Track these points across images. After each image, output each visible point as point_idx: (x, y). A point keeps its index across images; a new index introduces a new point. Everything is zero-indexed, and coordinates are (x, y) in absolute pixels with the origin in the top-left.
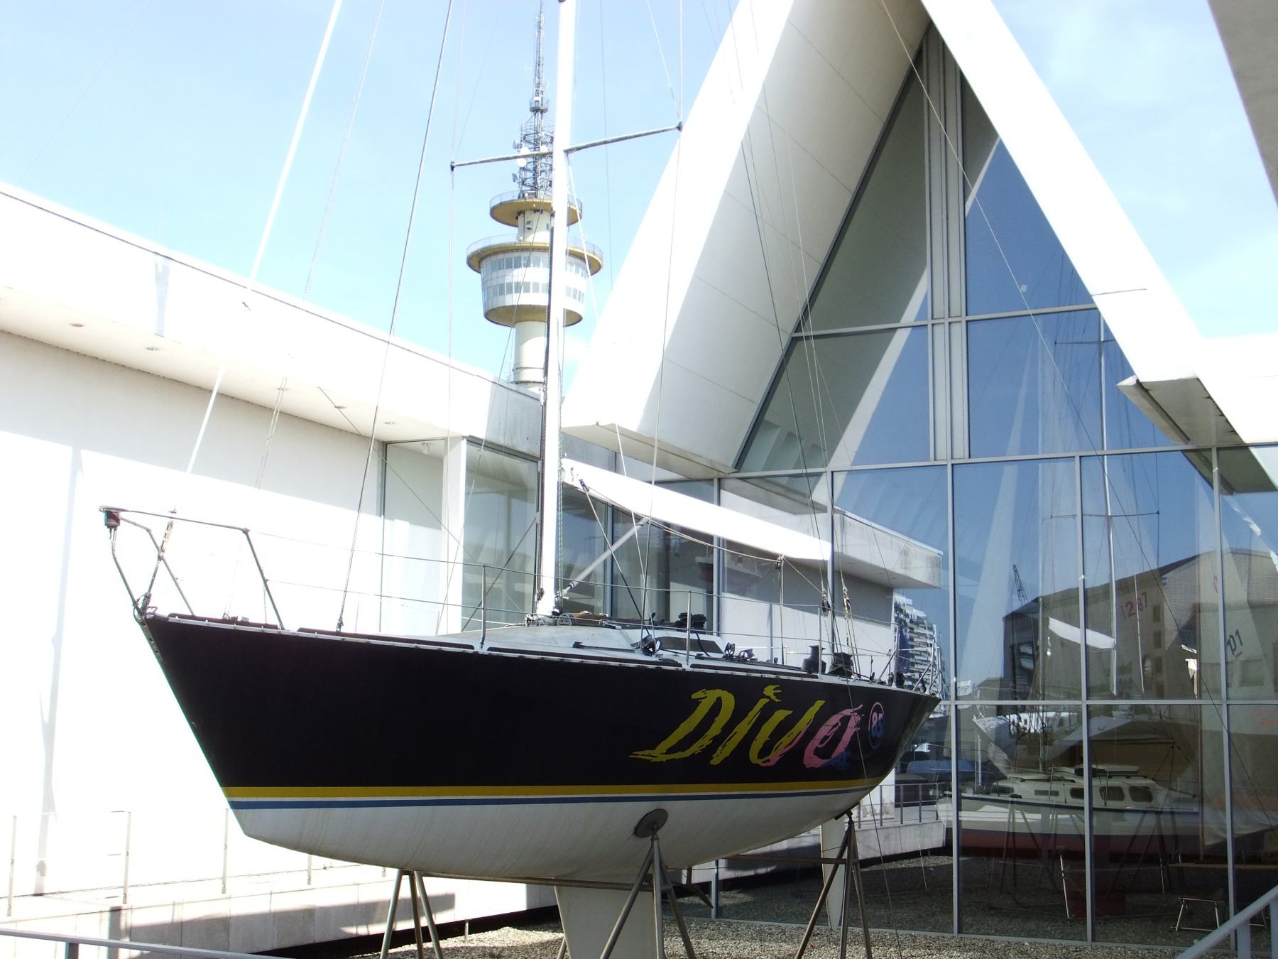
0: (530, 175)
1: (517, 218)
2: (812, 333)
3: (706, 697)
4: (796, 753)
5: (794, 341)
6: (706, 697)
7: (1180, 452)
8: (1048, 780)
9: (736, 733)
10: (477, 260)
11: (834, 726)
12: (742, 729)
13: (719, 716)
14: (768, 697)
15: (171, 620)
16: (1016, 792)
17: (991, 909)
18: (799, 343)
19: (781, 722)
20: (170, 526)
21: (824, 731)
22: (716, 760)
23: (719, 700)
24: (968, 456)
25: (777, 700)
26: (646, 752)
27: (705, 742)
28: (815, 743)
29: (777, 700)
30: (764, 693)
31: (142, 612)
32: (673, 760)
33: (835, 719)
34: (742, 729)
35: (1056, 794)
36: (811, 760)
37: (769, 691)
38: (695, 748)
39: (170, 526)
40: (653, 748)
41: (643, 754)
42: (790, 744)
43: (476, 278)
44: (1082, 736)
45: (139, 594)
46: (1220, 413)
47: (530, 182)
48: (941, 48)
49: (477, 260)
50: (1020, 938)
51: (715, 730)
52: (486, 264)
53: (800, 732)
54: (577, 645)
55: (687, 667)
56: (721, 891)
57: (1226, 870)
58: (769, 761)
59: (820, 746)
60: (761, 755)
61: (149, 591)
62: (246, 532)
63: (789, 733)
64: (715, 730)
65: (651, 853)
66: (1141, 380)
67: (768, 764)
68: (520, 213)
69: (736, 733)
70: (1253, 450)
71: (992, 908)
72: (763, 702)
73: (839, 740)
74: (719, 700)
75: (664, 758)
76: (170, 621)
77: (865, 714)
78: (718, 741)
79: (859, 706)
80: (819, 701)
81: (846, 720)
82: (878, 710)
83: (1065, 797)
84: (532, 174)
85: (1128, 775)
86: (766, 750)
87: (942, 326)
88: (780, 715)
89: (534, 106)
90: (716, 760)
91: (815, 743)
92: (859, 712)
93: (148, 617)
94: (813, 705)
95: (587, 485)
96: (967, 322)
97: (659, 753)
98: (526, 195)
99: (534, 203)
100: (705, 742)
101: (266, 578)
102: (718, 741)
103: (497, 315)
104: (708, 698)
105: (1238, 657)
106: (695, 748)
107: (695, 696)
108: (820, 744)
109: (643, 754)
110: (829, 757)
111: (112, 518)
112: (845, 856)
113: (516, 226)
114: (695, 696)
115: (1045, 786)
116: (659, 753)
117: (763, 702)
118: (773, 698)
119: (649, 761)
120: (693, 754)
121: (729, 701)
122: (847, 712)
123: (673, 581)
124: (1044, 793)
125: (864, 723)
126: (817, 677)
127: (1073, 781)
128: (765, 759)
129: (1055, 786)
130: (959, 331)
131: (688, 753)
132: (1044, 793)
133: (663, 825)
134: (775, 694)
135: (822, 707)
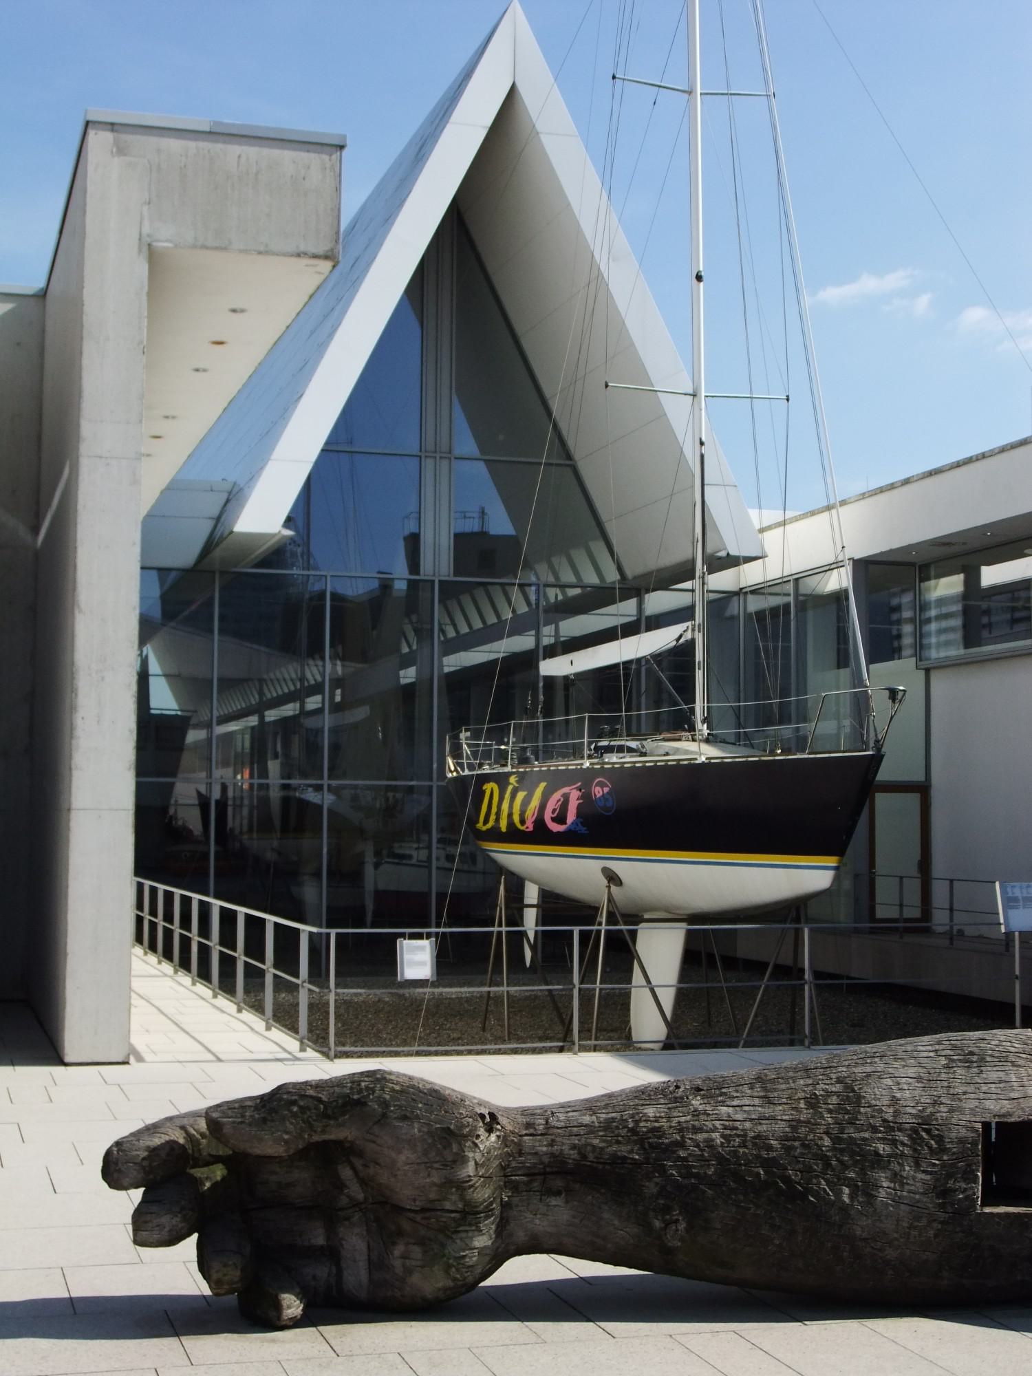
23: (492, 789)
33: (557, 796)
37: (513, 779)
64: (494, 810)
73: (566, 810)
81: (566, 798)
100: (493, 817)
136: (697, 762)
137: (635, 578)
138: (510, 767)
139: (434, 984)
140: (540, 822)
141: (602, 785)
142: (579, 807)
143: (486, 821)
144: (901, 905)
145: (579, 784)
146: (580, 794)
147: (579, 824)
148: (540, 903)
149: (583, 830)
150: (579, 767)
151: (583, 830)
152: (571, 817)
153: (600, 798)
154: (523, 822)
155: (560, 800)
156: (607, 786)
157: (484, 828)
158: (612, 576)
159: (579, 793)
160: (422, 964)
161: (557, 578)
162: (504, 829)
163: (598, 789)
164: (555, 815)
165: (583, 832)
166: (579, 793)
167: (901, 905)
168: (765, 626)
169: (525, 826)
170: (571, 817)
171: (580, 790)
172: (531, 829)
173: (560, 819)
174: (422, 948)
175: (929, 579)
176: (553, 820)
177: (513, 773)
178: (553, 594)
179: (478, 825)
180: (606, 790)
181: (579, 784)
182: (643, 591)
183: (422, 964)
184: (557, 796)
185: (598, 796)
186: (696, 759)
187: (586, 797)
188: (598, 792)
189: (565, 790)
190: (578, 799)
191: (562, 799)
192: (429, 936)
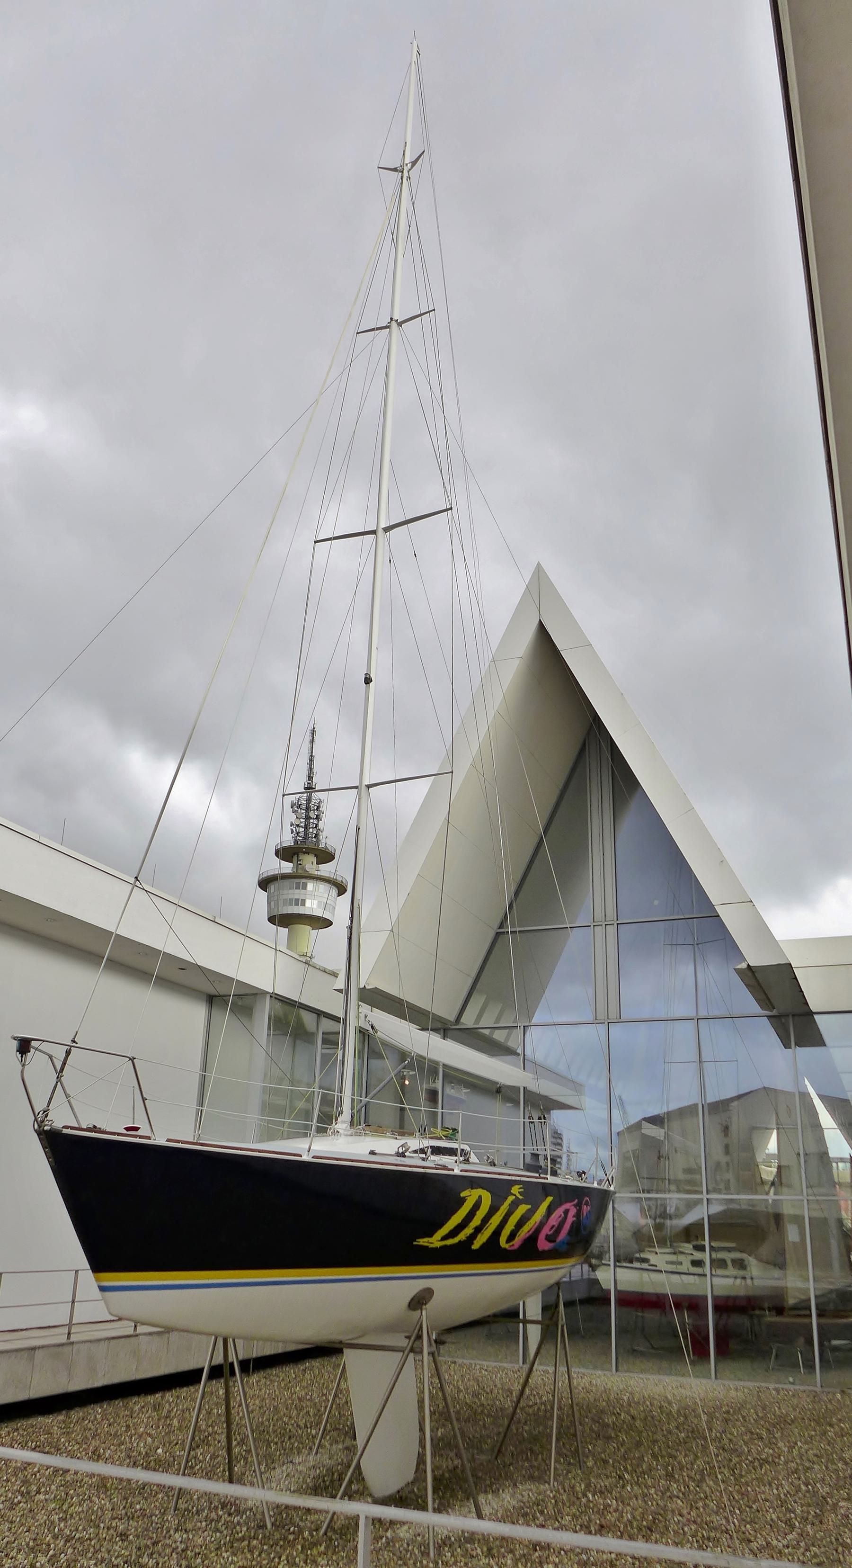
0: (302, 830)
1: (293, 857)
2: (518, 929)
3: (471, 1195)
4: (532, 1238)
5: (498, 934)
6: (471, 1195)
7: (766, 1018)
8: (675, 1253)
9: (491, 1224)
10: (264, 883)
12: (495, 1221)
13: (480, 1209)
14: (515, 1195)
15: (65, 1131)
16: (652, 1262)
17: (634, 1352)
18: (501, 936)
20: (68, 1053)
21: (554, 1220)
22: (476, 1245)
23: (480, 1197)
24: (619, 1017)
25: (521, 1197)
26: (426, 1240)
27: (468, 1231)
28: (546, 1231)
30: (512, 1191)
31: (41, 1124)
32: (446, 1246)
33: (560, 1211)
34: (495, 1221)
35: (681, 1263)
36: (543, 1245)
37: (516, 1190)
38: (462, 1236)
39: (68, 1053)
40: (431, 1235)
41: (423, 1242)
42: (529, 1231)
43: (263, 895)
45: (39, 1107)
47: (302, 834)
48: (609, 740)
49: (264, 883)
51: (476, 1221)
52: (272, 887)
54: (372, 1153)
55: (457, 1172)
57: (811, 1323)
58: (513, 1245)
59: (549, 1233)
60: (508, 1241)
61: (48, 1106)
62: (132, 1059)
64: (476, 1221)
65: (421, 1320)
66: (751, 964)
67: (513, 1248)
68: (294, 854)
70: (816, 1017)
71: (634, 1350)
72: (511, 1198)
74: (480, 1197)
75: (438, 1244)
76: (63, 1132)
77: (579, 1206)
78: (478, 1230)
79: (574, 1201)
81: (566, 1212)
82: (587, 1204)
83: (686, 1266)
84: (303, 830)
85: (729, 1250)
86: (512, 1237)
87: (600, 927)
88: (523, 1209)
89: (306, 786)
90: (476, 1245)
91: (546, 1231)
92: (575, 1206)
93: (46, 1128)
95: (377, 1027)
96: (618, 924)
97: (435, 1241)
98: (299, 843)
99: (304, 848)
100: (468, 1231)
101: (145, 1096)
102: (478, 1230)
103: (280, 920)
104: (471, 1196)
106: (462, 1236)
107: (463, 1195)
108: (550, 1230)
109: (423, 1242)
110: (554, 1241)
111: (24, 1046)
113: (292, 862)
114: (463, 1195)
115: (673, 1258)
116: (435, 1241)
117: (511, 1198)
118: (518, 1195)
119: (427, 1247)
120: (460, 1241)
122: (567, 1206)
124: (672, 1263)
125: (578, 1215)
126: (547, 1179)
127: (692, 1254)
128: (511, 1244)
129: (681, 1258)
130: (611, 930)
131: (456, 1240)
132: (672, 1263)
133: (430, 1300)
134: (519, 1192)
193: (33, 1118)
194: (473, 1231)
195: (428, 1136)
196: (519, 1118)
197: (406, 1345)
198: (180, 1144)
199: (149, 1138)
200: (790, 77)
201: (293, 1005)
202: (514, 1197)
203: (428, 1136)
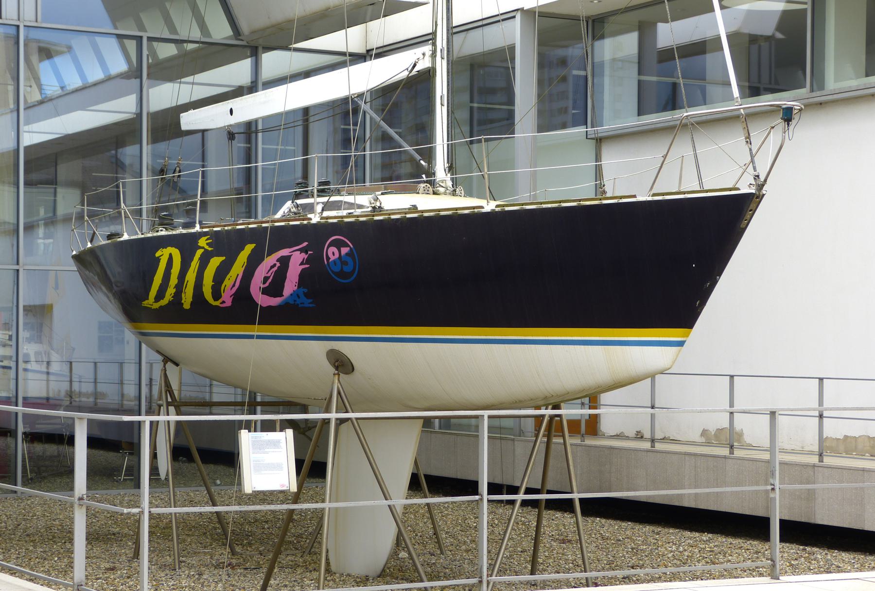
9: (188, 281)
11: (272, 267)
12: (191, 276)
14: (203, 248)
19: (218, 268)
23: (171, 255)
25: (210, 249)
27: (171, 291)
29: (210, 249)
30: (199, 244)
33: (270, 260)
34: (191, 276)
37: (203, 242)
42: (234, 285)
44: (220, 505)
46: (317, 448)
50: (193, 511)
51: (174, 280)
53: (238, 275)
56: (14, 430)
63: (228, 277)
64: (174, 280)
69: (188, 281)
72: (199, 252)
73: (284, 278)
74: (171, 255)
78: (180, 287)
80: (215, 258)
81: (285, 262)
88: (215, 262)
92: (303, 250)
94: (243, 249)
100: (171, 291)
104: (164, 254)
105: (20, 20)
107: (157, 255)
112: (170, 400)
117: (199, 252)
118: (207, 247)
121: (176, 253)
123: (232, 35)
134: (207, 244)
135: (253, 250)
136: (483, 210)
137: (253, 32)
138: (198, 226)
139: (296, 498)
140: (243, 294)
141: (338, 244)
142: (303, 276)
143: (160, 295)
144: (95, 382)
145: (306, 244)
146: (306, 256)
147: (302, 296)
148: (598, 396)
149: (307, 303)
150: (305, 222)
151: (307, 303)
152: (290, 287)
153: (334, 262)
154: (216, 295)
155: (275, 265)
156: (348, 246)
157: (156, 306)
158: (221, 31)
159: (304, 256)
160: (277, 467)
161: (172, 29)
162: (187, 305)
163: (333, 249)
164: (267, 284)
165: (307, 305)
166: (304, 256)
167: (95, 382)
168: (272, 166)
169: (220, 301)
170: (290, 287)
171: (306, 253)
172: (228, 303)
173: (274, 287)
174: (275, 444)
175: (602, 37)
176: (265, 292)
177: (205, 234)
178: (167, 51)
179: (145, 303)
180: (345, 250)
181: (306, 244)
182: (260, 49)
183: (277, 467)
184: (270, 260)
185: (332, 258)
186: (482, 207)
187: (315, 261)
188: (333, 253)
189: (284, 252)
190: (302, 264)
191: (278, 264)
192: (285, 425)
193: (755, 159)
194: (175, 290)
195: (475, 105)
196: (350, 129)
197: (150, 90)
198: (686, 195)
199: (634, 196)
200: (249, 97)
201: (203, 177)
202: (203, 250)
203: (475, 105)
